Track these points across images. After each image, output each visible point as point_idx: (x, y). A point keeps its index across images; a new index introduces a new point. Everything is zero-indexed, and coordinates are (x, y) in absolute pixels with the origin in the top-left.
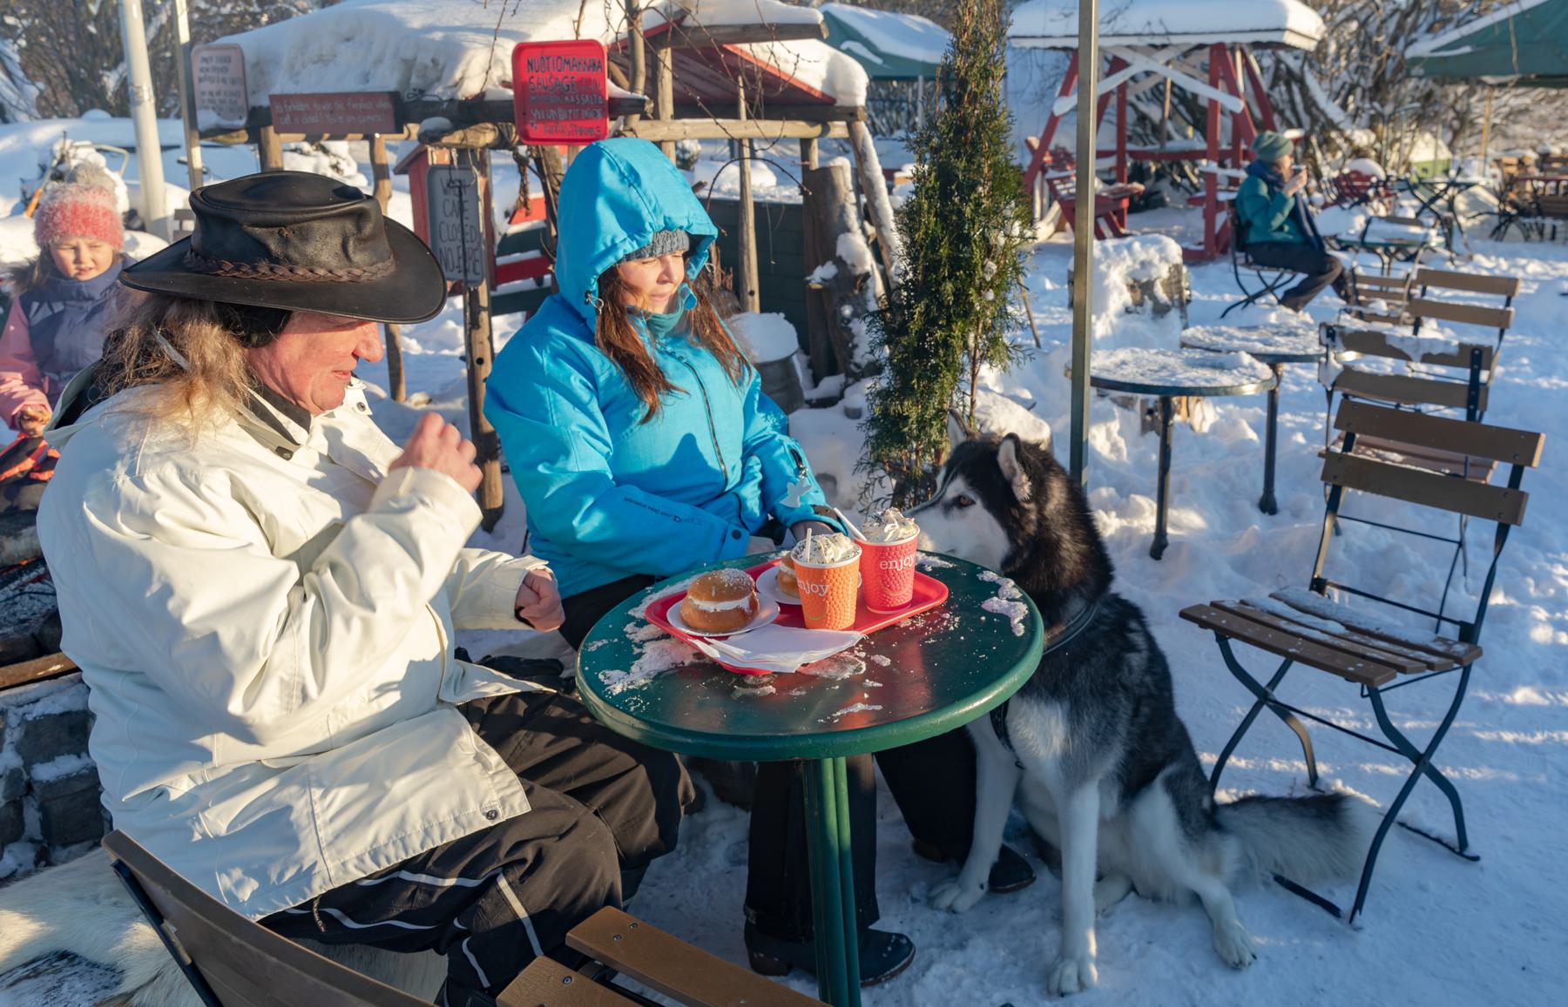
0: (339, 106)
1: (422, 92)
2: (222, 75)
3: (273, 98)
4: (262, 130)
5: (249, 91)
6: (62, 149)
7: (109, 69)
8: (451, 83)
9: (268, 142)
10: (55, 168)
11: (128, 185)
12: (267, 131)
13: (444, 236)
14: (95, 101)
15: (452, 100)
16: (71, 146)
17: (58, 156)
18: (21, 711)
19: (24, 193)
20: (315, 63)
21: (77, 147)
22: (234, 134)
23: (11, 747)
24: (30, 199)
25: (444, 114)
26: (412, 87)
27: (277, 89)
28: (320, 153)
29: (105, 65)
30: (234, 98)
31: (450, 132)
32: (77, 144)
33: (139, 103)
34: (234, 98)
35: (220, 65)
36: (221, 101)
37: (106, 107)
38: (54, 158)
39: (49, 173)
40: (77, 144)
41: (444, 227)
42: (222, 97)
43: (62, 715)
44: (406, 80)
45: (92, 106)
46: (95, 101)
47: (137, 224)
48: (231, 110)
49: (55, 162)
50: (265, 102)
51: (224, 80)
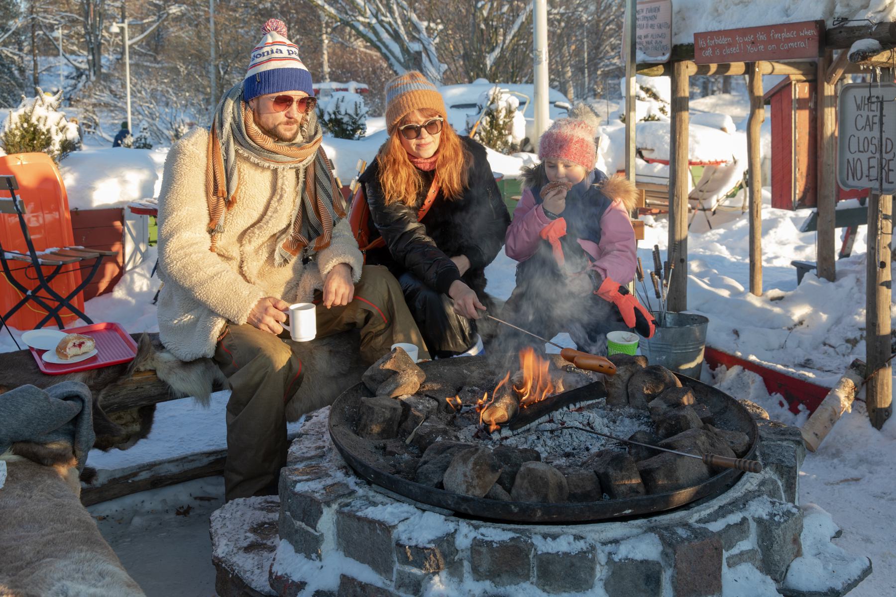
0: (762, 37)
1: (845, 20)
2: (650, 22)
3: (696, 35)
4: (676, 64)
5: (673, 34)
6: (494, 93)
7: (489, 53)
8: (881, 8)
9: (679, 74)
10: (488, 107)
11: (527, 121)
12: (679, 66)
13: (854, 147)
14: (480, 73)
15: (881, 23)
16: (499, 92)
17: (491, 99)
18: (609, 548)
19: (468, 124)
20: (736, 5)
21: (502, 93)
22: (655, 68)
23: (601, 584)
24: (471, 128)
25: (871, 36)
26: (836, 16)
27: (701, 27)
28: (652, 99)
29: (487, 50)
30: (659, 39)
31: (875, 52)
32: (502, 90)
33: (539, 63)
34: (659, 39)
35: (650, 14)
36: (648, 43)
37: (485, 76)
38: (489, 100)
39: (484, 111)
40: (502, 90)
41: (854, 141)
42: (649, 39)
43: (642, 562)
44: (831, 11)
45: (478, 76)
46: (480, 73)
47: (529, 148)
48: (656, 49)
49: (489, 103)
50: (691, 40)
51: (652, 26)
